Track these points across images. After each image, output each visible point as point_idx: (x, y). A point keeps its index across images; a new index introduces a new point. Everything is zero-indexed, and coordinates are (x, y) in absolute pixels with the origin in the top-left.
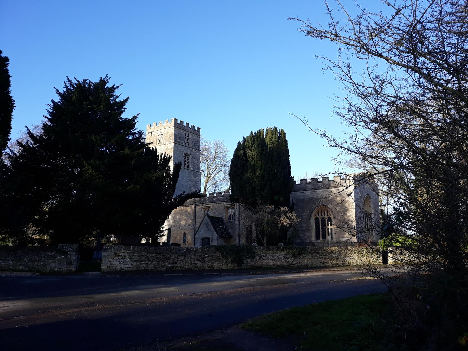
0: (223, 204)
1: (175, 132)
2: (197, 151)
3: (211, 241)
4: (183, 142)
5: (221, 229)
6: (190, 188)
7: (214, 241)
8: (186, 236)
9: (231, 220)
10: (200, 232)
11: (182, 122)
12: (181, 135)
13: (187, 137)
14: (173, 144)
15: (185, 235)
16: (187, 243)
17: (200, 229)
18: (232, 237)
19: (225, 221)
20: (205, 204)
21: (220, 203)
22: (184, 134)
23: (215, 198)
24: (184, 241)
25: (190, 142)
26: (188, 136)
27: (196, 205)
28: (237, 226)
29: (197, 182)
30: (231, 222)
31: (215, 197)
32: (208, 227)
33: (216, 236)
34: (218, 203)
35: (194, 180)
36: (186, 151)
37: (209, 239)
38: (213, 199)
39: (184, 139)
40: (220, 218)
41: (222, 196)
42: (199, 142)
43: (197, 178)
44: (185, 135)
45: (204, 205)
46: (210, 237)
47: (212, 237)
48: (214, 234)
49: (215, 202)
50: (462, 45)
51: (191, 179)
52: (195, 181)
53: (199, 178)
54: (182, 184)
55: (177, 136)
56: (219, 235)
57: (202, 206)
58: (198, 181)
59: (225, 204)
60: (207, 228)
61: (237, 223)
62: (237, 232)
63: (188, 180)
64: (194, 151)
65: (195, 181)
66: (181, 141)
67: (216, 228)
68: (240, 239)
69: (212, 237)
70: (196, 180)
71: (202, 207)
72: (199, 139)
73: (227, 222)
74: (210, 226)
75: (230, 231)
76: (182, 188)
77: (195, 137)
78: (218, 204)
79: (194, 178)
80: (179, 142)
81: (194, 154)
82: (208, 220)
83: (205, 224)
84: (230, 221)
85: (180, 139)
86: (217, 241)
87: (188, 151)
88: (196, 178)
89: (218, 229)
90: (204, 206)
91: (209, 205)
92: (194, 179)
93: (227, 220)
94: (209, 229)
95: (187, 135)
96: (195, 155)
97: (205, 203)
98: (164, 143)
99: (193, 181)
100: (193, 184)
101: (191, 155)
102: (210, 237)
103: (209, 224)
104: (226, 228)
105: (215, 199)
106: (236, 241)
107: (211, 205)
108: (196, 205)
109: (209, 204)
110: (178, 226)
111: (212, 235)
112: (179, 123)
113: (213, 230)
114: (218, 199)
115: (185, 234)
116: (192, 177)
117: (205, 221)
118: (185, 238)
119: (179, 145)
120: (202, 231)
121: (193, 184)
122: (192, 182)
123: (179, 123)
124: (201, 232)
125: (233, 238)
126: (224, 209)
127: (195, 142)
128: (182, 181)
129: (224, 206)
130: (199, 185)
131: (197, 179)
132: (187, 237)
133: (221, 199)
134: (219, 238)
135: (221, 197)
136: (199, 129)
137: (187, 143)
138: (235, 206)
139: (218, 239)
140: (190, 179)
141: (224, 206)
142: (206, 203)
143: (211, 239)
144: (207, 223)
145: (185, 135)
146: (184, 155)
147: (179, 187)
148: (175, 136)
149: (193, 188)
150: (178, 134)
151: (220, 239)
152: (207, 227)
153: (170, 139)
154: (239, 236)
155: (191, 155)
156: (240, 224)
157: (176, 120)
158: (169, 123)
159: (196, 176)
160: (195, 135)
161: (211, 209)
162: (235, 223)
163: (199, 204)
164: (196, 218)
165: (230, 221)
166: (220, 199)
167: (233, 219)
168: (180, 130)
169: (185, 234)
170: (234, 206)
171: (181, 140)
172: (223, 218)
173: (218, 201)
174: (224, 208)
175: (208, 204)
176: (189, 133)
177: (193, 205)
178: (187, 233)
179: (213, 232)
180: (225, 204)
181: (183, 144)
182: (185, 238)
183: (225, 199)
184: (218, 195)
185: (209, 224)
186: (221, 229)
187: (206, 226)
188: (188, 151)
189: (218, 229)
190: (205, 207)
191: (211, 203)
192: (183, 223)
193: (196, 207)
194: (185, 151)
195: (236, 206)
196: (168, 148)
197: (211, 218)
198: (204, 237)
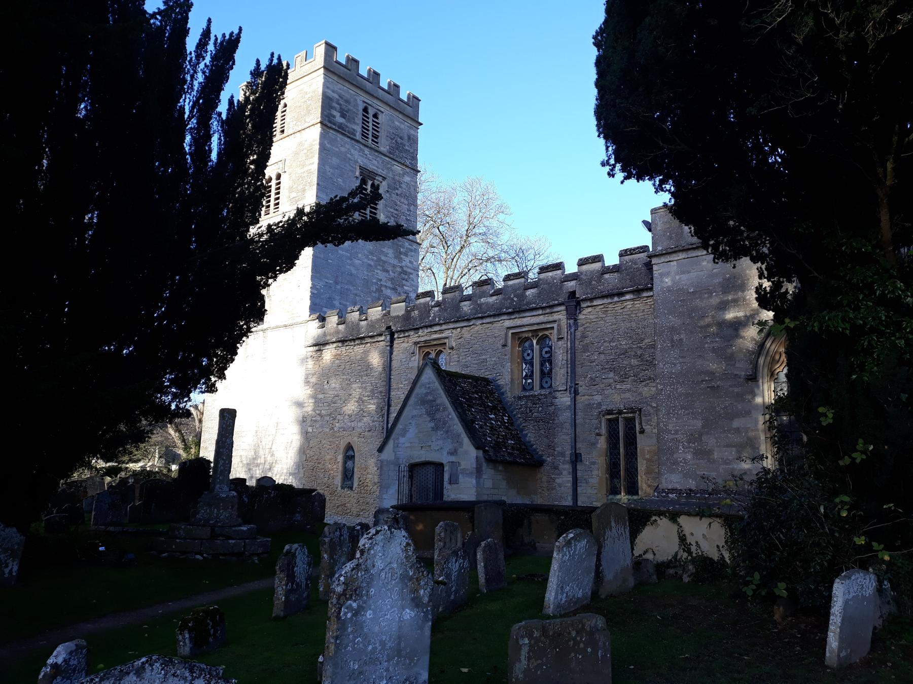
0: (499, 324)
1: (325, 86)
2: (408, 170)
3: (446, 477)
4: (358, 129)
5: (492, 428)
6: (379, 290)
7: (460, 476)
8: (354, 456)
9: (537, 390)
10: (402, 440)
11: (353, 62)
12: (347, 101)
13: (370, 116)
14: (318, 129)
15: (349, 454)
16: (355, 485)
17: (400, 426)
18: (538, 464)
19: (509, 396)
20: (426, 331)
21: (488, 320)
22: (361, 107)
23: (467, 303)
24: (348, 476)
25: (383, 135)
26: (375, 116)
27: (392, 334)
28: (566, 416)
29: (405, 273)
30: (535, 400)
31: (469, 298)
32: (438, 416)
33: (469, 454)
34: (479, 322)
35: (394, 266)
36: (365, 161)
37: (439, 467)
38: (457, 308)
39: (359, 120)
40: (487, 381)
41: (498, 292)
42: (414, 141)
43: (407, 260)
44: (365, 110)
45: (424, 335)
46: (444, 458)
47: (453, 458)
48: (461, 444)
49: (468, 320)
50: (748, 235)
51: (385, 262)
52: (399, 269)
53: (411, 262)
54: (351, 275)
55: (334, 105)
56: (485, 451)
57: (414, 337)
58: (409, 270)
59: (508, 323)
60: (433, 419)
61: (564, 400)
62: (563, 441)
63: (372, 263)
64: (398, 168)
65: (399, 269)
66: (349, 124)
67: (473, 422)
68: (579, 474)
69: (453, 458)
70: (401, 267)
71: (416, 343)
72: (412, 132)
73: (520, 398)
74: (445, 409)
75: (531, 435)
76: (352, 288)
77: (404, 126)
78: (478, 327)
79: (395, 257)
80: (341, 126)
81: (397, 178)
82: (437, 385)
83: (423, 402)
84: (532, 393)
85: (343, 116)
86: (474, 481)
87: (375, 162)
88: (400, 260)
89: (481, 427)
90: (423, 339)
91: (441, 331)
92: (395, 262)
93: (518, 392)
94: (439, 425)
95: (371, 112)
96: (400, 183)
97: (427, 327)
98: (291, 132)
99: (390, 269)
100: (392, 279)
101: (384, 178)
102: (444, 462)
103: (438, 402)
104: (512, 424)
105: (466, 307)
106: (558, 481)
107: (452, 335)
108: (392, 334)
109: (444, 327)
110: (327, 418)
111: (453, 453)
112: (343, 61)
113: (458, 428)
114: (480, 305)
115: (349, 447)
116: (386, 255)
117: (424, 391)
118: (349, 464)
119: (341, 136)
120: (412, 432)
121: (392, 279)
122: (388, 271)
123: (343, 61)
124: (403, 436)
125: (546, 468)
126: (504, 346)
127: (401, 138)
128: (348, 261)
129: (506, 335)
130: (412, 286)
131: (404, 264)
132: (356, 459)
133: (490, 306)
134: (484, 464)
135: (492, 295)
136: (414, 101)
137: (370, 136)
138: (555, 330)
139: (479, 471)
140: (379, 260)
141: (506, 335)
142: (431, 326)
143: (446, 468)
144: (430, 398)
145: (365, 110)
146: (358, 174)
147: (336, 283)
148: (327, 102)
149: (389, 291)
150: (337, 97)
151: (489, 473)
152: (431, 414)
153: (309, 112)
154: (576, 458)
155: (384, 178)
156: (579, 406)
157: (331, 49)
158: (308, 62)
159: (401, 253)
160: (400, 116)
161: (452, 348)
162: (552, 404)
163: (404, 331)
164: (394, 385)
165: (532, 393)
166: (487, 304)
167: (542, 387)
168: (347, 85)
169: (349, 447)
170: (547, 333)
171: (349, 121)
172: (501, 382)
173: (482, 314)
174: (502, 342)
175: (437, 328)
176: (379, 103)
177: (381, 335)
178: (356, 441)
179: (459, 436)
180: (508, 323)
181: (355, 135)
182: (349, 464)
183: (507, 303)
184: (478, 290)
185: (438, 402)
186: (492, 428)
187: (429, 414)
188: (374, 164)
189: (481, 427)
190: (425, 341)
191: (452, 326)
192: (351, 407)
193: (391, 346)
194: (361, 162)
195: (559, 331)
196: (300, 144)
197: (449, 379)
198: (417, 460)
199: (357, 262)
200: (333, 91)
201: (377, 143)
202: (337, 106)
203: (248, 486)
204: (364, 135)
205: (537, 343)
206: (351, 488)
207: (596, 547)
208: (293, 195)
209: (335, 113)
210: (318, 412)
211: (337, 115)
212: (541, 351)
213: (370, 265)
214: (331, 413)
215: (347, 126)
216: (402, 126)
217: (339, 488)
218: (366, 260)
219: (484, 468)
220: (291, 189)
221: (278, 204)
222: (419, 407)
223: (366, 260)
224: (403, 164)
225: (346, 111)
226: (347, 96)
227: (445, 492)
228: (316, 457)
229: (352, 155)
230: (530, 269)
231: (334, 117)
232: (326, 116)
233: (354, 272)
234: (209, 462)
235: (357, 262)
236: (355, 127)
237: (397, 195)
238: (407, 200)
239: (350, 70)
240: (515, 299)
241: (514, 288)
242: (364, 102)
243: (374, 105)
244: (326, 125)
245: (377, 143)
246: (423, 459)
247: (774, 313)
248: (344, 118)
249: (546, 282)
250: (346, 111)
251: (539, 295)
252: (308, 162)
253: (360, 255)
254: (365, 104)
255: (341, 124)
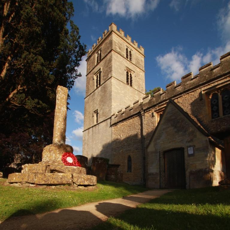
12: (121, 44)
16: (132, 170)
22: (126, 47)
54: (125, 102)
55: (117, 44)
81: (138, 73)
85: (120, 49)
87: (131, 66)
96: (139, 75)
128: (124, 98)
145: (127, 49)
147: (120, 105)
160: (138, 53)
171: (121, 51)
176: (132, 47)
188: (131, 67)
194: (127, 65)
199: (126, 98)
200: (116, 40)
202: (118, 45)
203: (57, 86)
204: (127, 57)
205: (220, 94)
206: (131, 172)
209: (117, 47)
212: (222, 97)
213: (131, 100)
216: (139, 56)
217: (126, 172)
218: (130, 98)
219: (209, 147)
220: (104, 77)
222: (166, 124)
223: (130, 98)
224: (140, 69)
226: (121, 43)
227: (186, 162)
229: (123, 62)
231: (117, 49)
233: (126, 102)
235: (126, 98)
236: (124, 54)
237: (138, 78)
238: (142, 80)
239: (121, 34)
240: (207, 76)
241: (206, 72)
242: (126, 46)
243: (129, 47)
246: (171, 148)
249: (227, 61)
251: (221, 70)
253: (128, 96)
254: (127, 47)
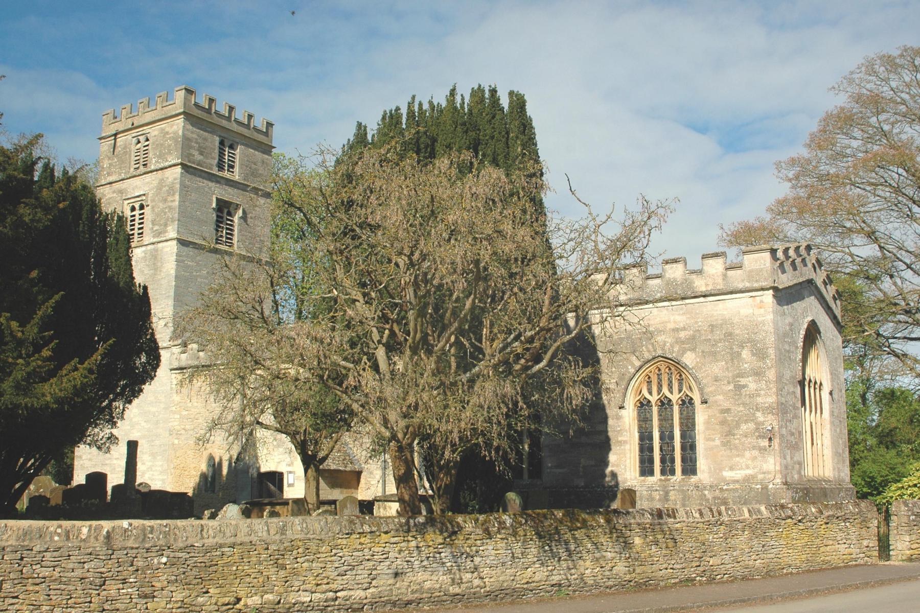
85: (201, 153)
98: (153, 167)
171: (206, 157)
201: (233, 172)
207: (188, 486)
208: (156, 228)
210: (183, 427)
211: (196, 153)
214: (194, 428)
215: (205, 163)
217: (203, 492)
221: (142, 233)
225: (205, 149)
228: (182, 465)
230: (450, 168)
232: (186, 156)
234: (70, 484)
244: (186, 165)
245: (233, 172)
247: (190, 494)
248: (202, 155)
250: (205, 149)
252: (170, 199)
255: (199, 161)
